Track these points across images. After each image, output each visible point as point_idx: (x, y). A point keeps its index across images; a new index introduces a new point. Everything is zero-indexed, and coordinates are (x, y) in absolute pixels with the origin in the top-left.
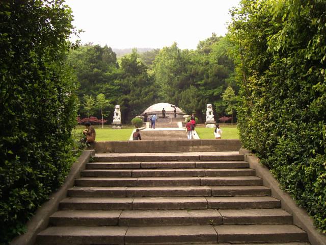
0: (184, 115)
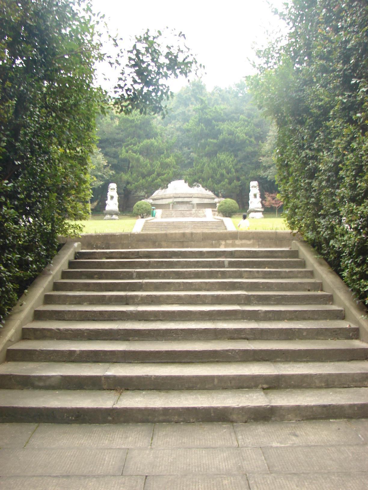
0: (214, 199)
